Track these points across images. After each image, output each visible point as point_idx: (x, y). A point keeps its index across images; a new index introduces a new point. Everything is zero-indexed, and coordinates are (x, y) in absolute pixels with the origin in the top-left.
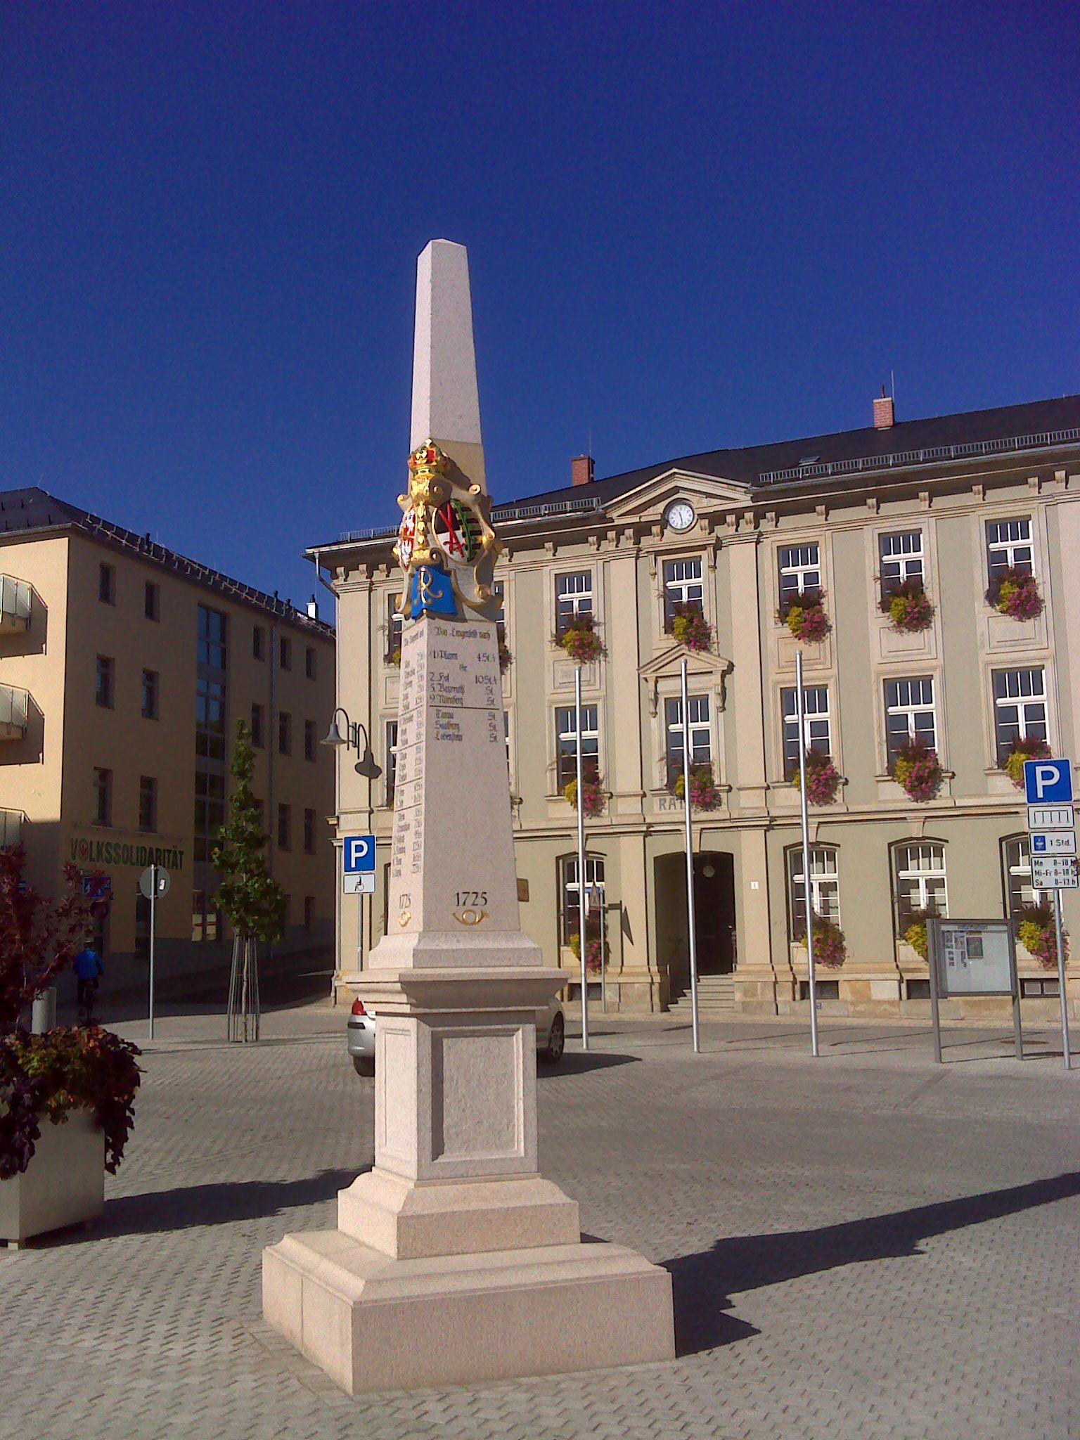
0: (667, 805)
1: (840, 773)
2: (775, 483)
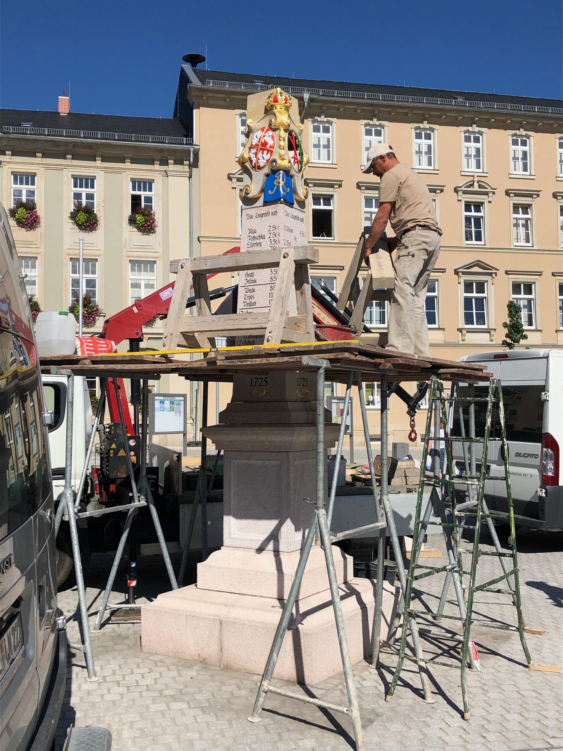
2: (13, 133)
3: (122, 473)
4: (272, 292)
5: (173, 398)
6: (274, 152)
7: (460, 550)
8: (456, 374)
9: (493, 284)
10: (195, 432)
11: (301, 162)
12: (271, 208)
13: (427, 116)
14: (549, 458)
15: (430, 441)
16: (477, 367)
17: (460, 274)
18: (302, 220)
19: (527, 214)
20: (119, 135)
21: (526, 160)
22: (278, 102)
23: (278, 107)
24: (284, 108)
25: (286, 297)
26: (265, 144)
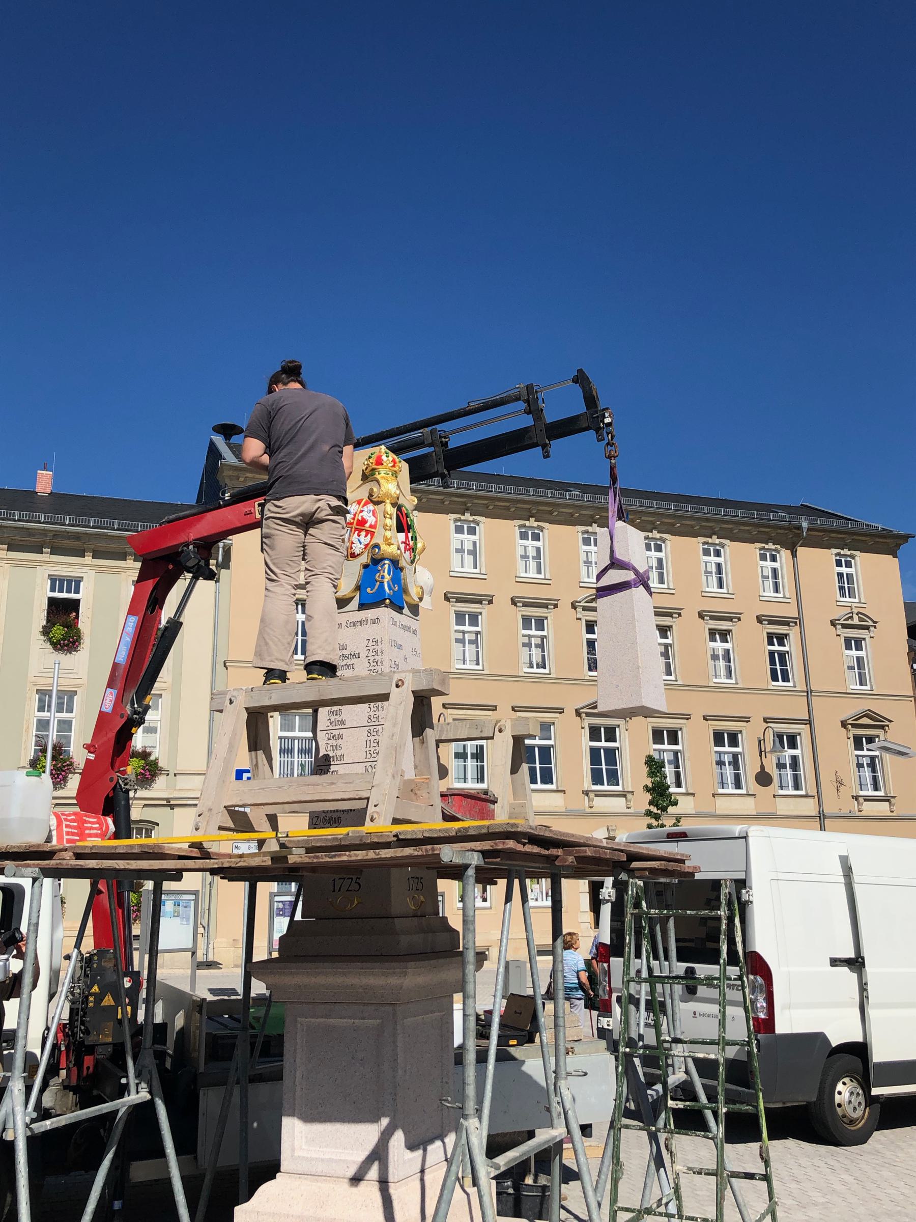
3: (106, 1036)
4: (370, 738)
5: (179, 897)
6: (375, 534)
7: (678, 1167)
8: (657, 869)
9: (627, 730)
10: (206, 947)
11: (413, 550)
12: (370, 614)
13: (534, 512)
14: (758, 990)
15: (631, 983)
16: (679, 857)
17: (584, 715)
18: (415, 632)
19: (667, 638)
20: (119, 523)
21: (662, 569)
22: (382, 464)
23: (382, 472)
24: (391, 473)
25: (400, 747)
26: (363, 522)
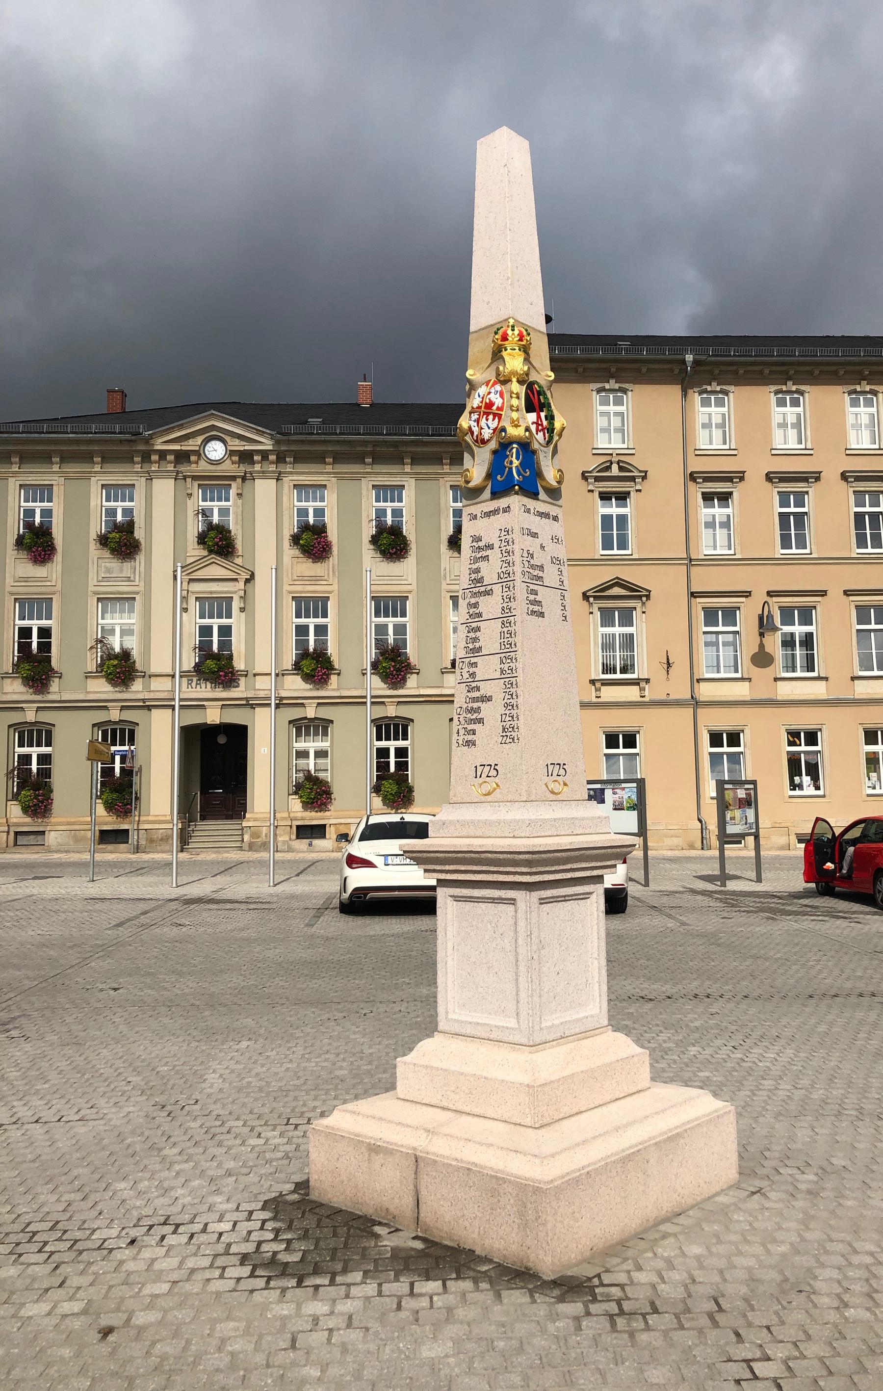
0: (194, 684)
1: (336, 666)
11: (551, 430)
12: (503, 502)
18: (556, 518)
26: (490, 405)
